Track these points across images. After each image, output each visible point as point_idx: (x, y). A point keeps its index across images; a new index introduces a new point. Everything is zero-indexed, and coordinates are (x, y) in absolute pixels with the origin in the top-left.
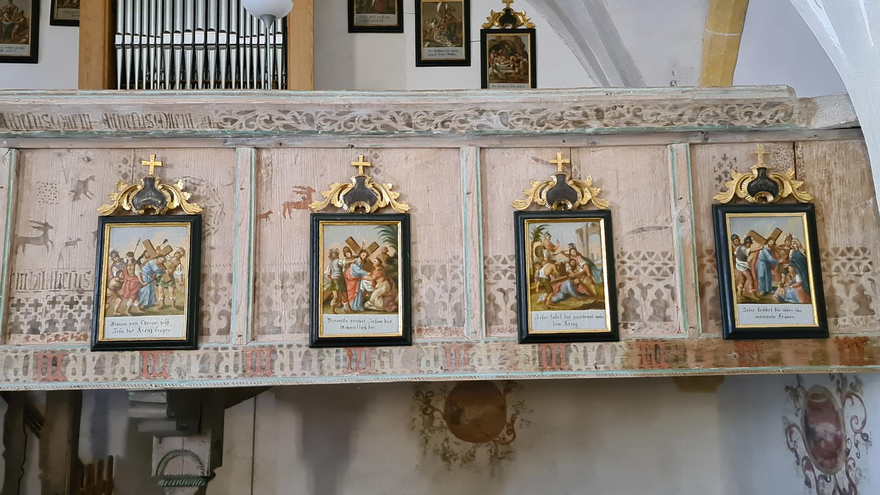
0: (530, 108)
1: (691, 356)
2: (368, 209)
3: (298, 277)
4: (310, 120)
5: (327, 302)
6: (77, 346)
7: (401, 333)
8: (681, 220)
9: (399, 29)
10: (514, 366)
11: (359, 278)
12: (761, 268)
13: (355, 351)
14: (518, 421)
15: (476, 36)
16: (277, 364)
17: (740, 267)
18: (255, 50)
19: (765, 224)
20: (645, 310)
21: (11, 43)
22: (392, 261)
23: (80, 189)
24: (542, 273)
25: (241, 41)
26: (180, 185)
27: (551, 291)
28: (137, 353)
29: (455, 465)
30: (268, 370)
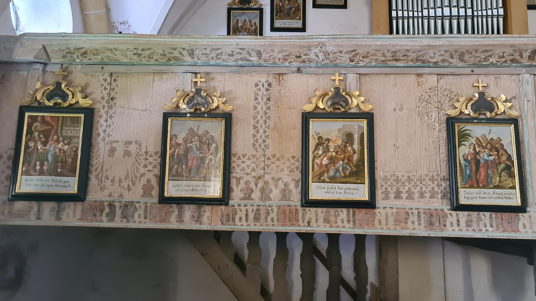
7: (76, 191)
16: (237, 218)
18: (485, 19)
21: (291, 19)
25: (475, 13)
26: (218, 94)
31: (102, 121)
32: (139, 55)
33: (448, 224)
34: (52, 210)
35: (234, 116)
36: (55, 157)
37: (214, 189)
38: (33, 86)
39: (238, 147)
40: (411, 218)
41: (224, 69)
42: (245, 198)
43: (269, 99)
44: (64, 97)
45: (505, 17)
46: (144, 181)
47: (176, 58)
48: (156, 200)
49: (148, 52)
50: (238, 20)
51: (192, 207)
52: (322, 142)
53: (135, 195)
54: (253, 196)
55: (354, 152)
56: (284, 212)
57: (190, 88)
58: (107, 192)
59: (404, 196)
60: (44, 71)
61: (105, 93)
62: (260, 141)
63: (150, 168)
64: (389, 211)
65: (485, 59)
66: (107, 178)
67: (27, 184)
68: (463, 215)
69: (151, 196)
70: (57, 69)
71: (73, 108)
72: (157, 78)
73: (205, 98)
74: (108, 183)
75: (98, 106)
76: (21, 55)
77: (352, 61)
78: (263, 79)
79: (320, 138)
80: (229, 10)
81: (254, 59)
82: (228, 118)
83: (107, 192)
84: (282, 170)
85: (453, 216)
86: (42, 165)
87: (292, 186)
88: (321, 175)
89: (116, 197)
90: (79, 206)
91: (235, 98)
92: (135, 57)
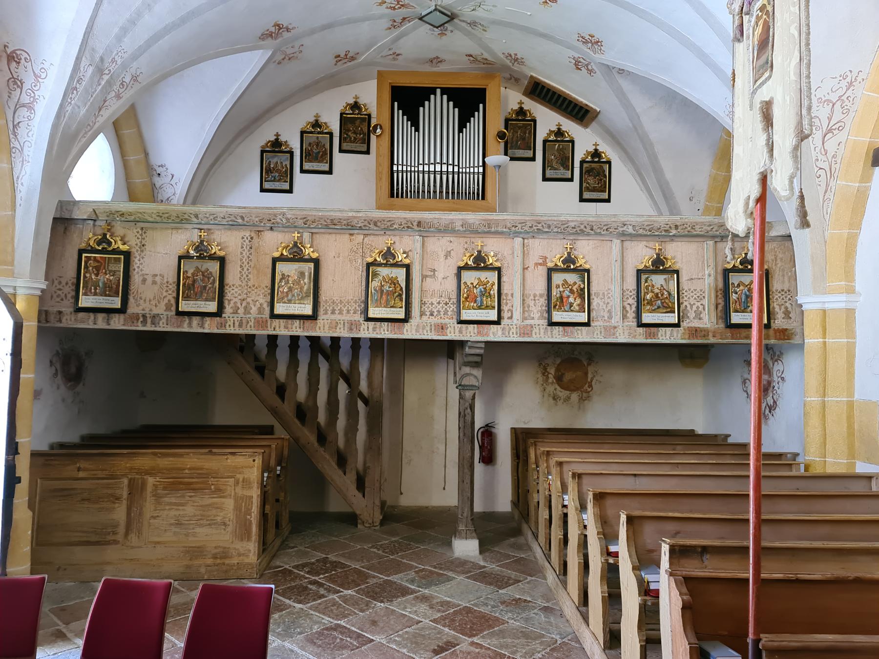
1: (711, 335)
2: (572, 267)
3: (541, 296)
4: (549, 227)
5: (555, 307)
6: (452, 323)
8: (710, 275)
9: (533, 159)
10: (635, 337)
11: (568, 297)
12: (743, 297)
13: (566, 328)
14: (594, 381)
15: (577, 164)
17: (734, 297)
20: (692, 315)
22: (583, 290)
24: (648, 297)
29: (560, 403)
31: (136, 260)
34: (104, 318)
35: (227, 259)
36: (105, 284)
37: (212, 307)
38: (88, 236)
40: (339, 326)
41: (220, 227)
44: (109, 244)
46: (166, 301)
48: (174, 313)
51: (198, 318)
52: (283, 277)
53: (160, 310)
54: (239, 311)
56: (258, 322)
57: (196, 239)
58: (141, 308)
59: (337, 312)
60: (94, 225)
61: (138, 241)
63: (170, 292)
65: (391, 226)
66: (141, 298)
67: (85, 301)
68: (371, 324)
69: (171, 311)
70: (103, 223)
71: (116, 251)
72: (174, 232)
74: (142, 302)
75: (133, 250)
76: (77, 214)
79: (283, 275)
80: (262, 152)
81: (240, 221)
82: (222, 261)
83: (141, 308)
88: (283, 298)
89: (147, 311)
90: (122, 316)
91: (226, 247)
92: (158, 218)
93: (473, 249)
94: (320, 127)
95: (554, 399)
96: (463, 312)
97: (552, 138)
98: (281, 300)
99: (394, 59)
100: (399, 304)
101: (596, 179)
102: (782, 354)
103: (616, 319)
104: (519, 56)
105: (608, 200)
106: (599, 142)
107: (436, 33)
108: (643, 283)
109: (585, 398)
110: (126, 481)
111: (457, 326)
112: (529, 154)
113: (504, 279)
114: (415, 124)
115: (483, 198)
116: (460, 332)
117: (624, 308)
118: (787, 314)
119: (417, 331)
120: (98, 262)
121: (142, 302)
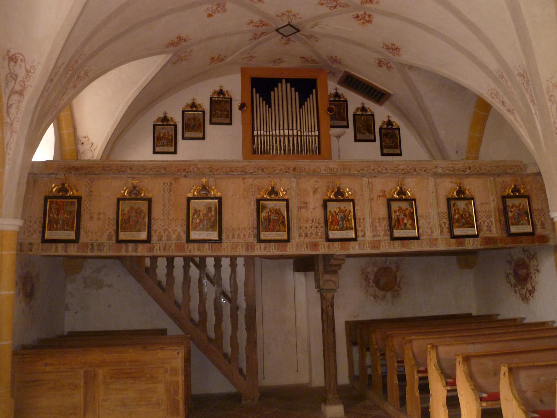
0: (451, 166)
1: (499, 242)
2: (404, 197)
3: (384, 219)
4: (386, 169)
5: (395, 226)
6: (322, 241)
8: (494, 201)
9: (347, 127)
10: (450, 246)
11: (403, 219)
12: (516, 215)
13: (404, 241)
14: (402, 282)
15: (377, 130)
16: (155, 249)
17: (510, 214)
19: (517, 202)
20: (485, 228)
23: (315, 191)
24: (456, 217)
25: (302, 134)
27: (459, 222)
28: (339, 243)
30: (378, 247)
32: (105, 170)
33: (256, 249)
37: (143, 236)
39: (154, 215)
40: (239, 247)
42: (159, 240)
43: (170, 191)
45: (319, 137)
46: (108, 233)
47: (124, 171)
48: (114, 241)
49: (109, 169)
50: (160, 132)
52: (196, 211)
53: (104, 239)
54: (163, 239)
55: (212, 216)
59: (236, 237)
62: (166, 212)
63: (111, 226)
64: (228, 244)
65: (274, 171)
68: (263, 245)
73: (138, 191)
77: (211, 172)
78: (168, 181)
79: (195, 210)
80: (155, 126)
81: (163, 171)
82: (150, 201)
84: (177, 226)
85: (258, 246)
86: (57, 225)
87: (182, 234)
88: (196, 228)
90: (76, 245)
93: (333, 187)
94: (196, 107)
95: (375, 297)
96: (330, 232)
97: (359, 112)
98: (195, 229)
99: (250, 60)
100: (283, 229)
101: (391, 140)
102: (535, 254)
103: (436, 234)
104: (338, 58)
105: (400, 154)
106: (391, 115)
107: (282, 43)
108: (452, 207)
109: (396, 296)
110: (82, 372)
111: (325, 243)
112: (345, 123)
113: (356, 208)
114: (269, 103)
115: (319, 153)
116: (329, 248)
117: (441, 225)
118: (543, 224)
119: (297, 248)
120: (59, 205)
121: (90, 234)
